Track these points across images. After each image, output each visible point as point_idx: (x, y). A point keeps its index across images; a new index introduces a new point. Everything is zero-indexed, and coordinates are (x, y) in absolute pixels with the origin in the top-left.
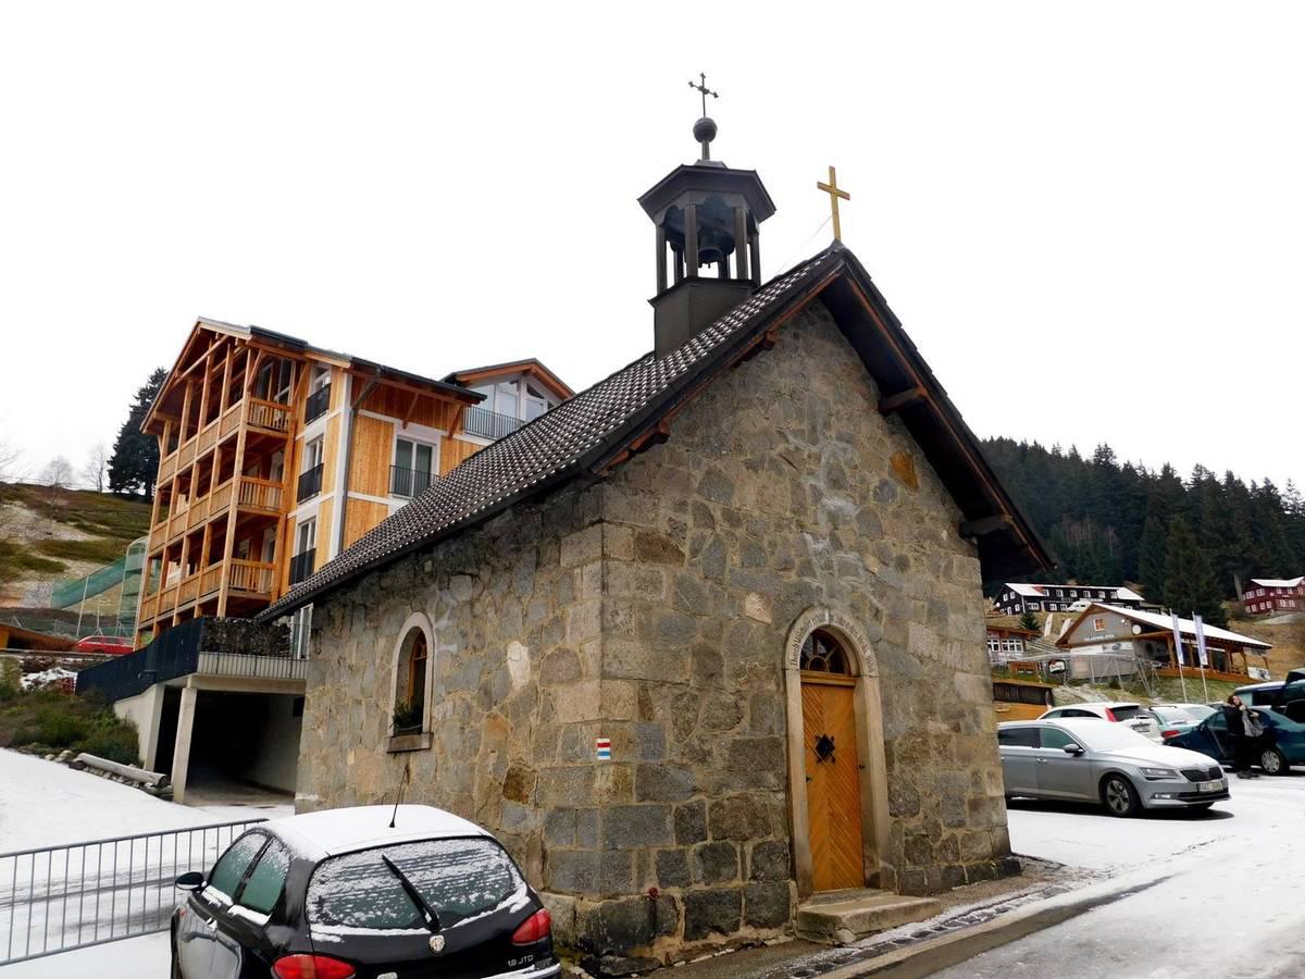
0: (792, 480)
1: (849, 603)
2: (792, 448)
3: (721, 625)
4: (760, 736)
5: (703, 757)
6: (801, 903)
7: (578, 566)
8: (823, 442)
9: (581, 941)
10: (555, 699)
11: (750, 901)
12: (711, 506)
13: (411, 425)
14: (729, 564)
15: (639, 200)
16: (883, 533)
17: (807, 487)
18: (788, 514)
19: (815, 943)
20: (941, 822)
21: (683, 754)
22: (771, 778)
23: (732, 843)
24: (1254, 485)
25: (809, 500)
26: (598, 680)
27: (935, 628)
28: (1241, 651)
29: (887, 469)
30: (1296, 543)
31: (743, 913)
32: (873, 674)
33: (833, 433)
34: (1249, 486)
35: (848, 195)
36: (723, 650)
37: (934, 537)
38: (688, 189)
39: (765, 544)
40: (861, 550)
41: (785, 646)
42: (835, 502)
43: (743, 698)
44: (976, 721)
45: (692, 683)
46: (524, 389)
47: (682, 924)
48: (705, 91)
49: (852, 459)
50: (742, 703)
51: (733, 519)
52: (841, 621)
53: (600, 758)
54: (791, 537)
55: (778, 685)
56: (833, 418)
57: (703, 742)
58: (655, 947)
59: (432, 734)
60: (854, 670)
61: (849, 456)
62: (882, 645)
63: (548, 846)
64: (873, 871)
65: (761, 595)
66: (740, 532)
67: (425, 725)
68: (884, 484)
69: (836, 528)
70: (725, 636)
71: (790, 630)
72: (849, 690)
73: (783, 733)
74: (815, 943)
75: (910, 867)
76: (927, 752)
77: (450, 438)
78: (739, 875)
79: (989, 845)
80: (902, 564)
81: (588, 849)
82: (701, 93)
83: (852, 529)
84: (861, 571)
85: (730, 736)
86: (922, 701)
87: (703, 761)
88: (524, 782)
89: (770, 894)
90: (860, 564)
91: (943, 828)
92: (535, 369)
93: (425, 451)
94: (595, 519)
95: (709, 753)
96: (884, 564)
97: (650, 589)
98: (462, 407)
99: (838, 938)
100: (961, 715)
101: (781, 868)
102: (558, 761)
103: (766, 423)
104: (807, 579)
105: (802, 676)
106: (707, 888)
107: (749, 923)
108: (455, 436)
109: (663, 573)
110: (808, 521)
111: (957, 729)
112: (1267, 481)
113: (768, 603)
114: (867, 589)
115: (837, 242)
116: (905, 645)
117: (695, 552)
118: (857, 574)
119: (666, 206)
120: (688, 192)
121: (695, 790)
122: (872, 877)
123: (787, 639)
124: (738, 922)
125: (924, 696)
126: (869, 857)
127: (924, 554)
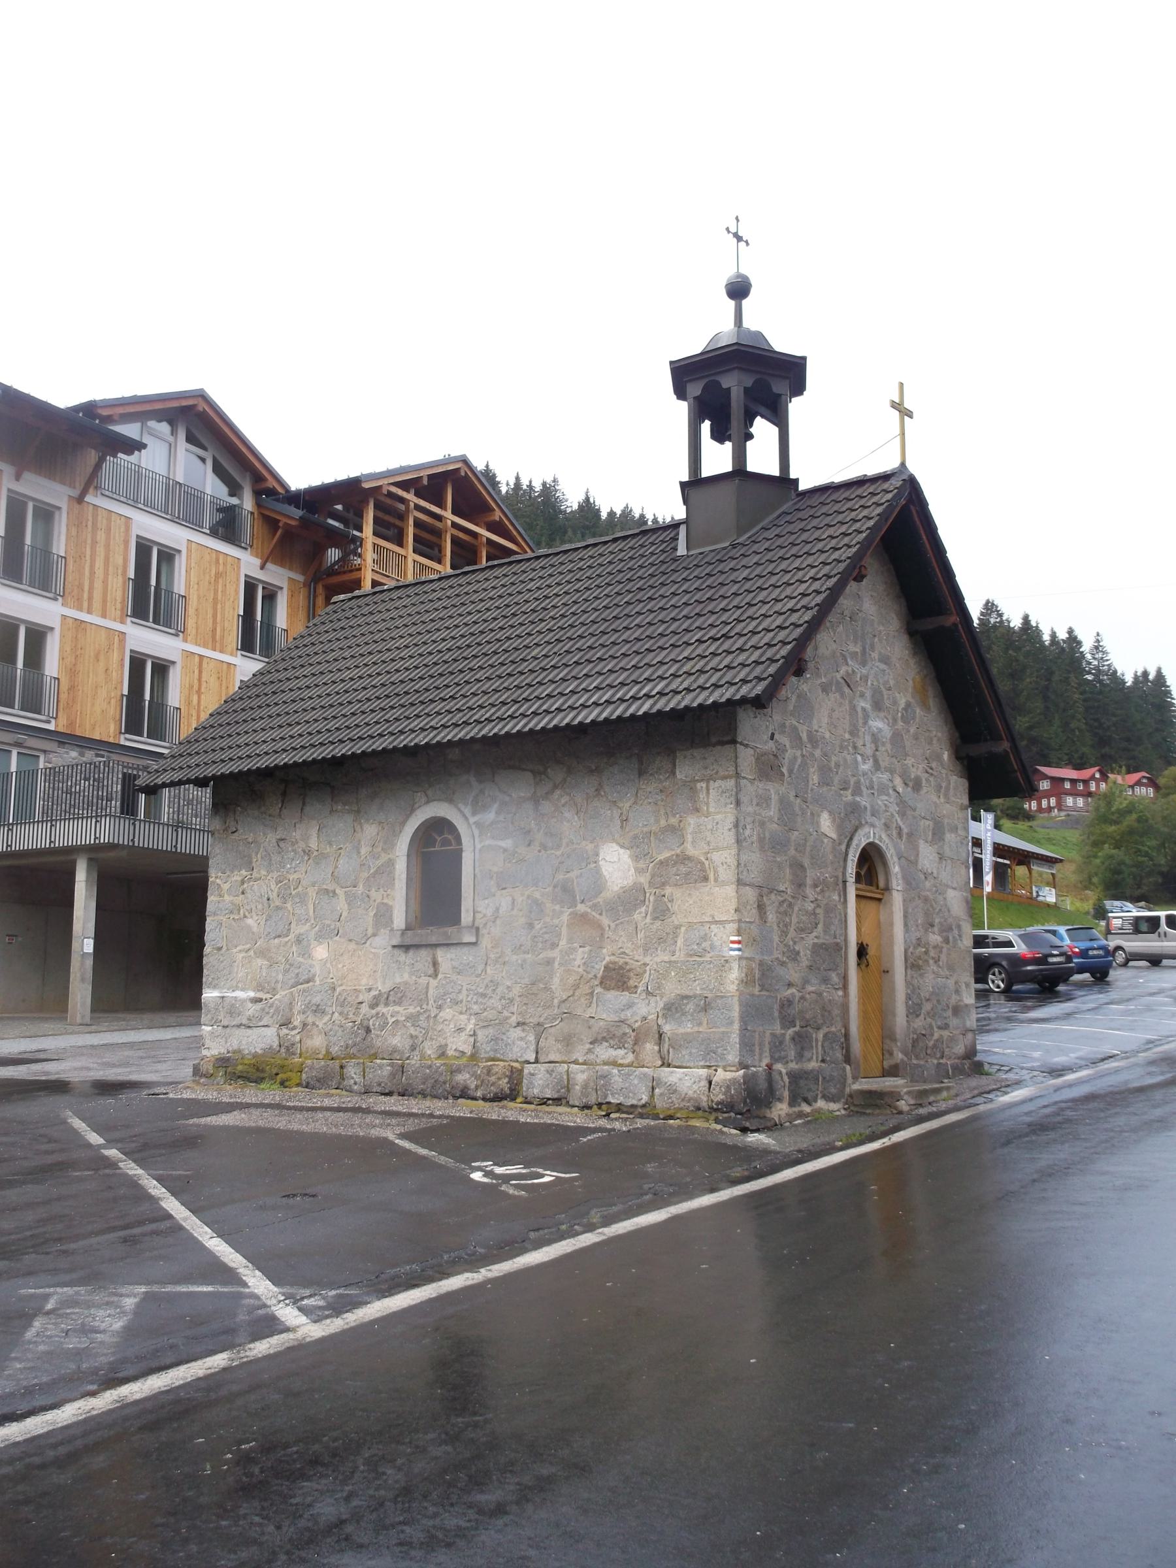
0: (850, 702)
1: (883, 821)
2: (850, 669)
3: (805, 840)
4: (829, 940)
5: (794, 956)
6: (854, 1083)
7: (702, 780)
8: (870, 664)
9: (718, 1103)
10: (671, 901)
11: (824, 1078)
12: (800, 727)
13: (27, 476)
14: (811, 782)
15: (671, 363)
16: (907, 755)
17: (859, 710)
18: (847, 736)
19: (864, 1113)
20: (934, 1024)
21: (784, 953)
22: (834, 977)
23: (811, 1030)
24: (1053, 635)
25: (861, 721)
26: (734, 886)
27: (936, 846)
28: (1028, 865)
29: (910, 690)
30: (1095, 720)
31: (820, 1089)
32: (899, 888)
33: (875, 655)
34: (1046, 638)
35: (893, 407)
36: (806, 862)
37: (938, 758)
38: (740, 369)
39: (833, 764)
40: (892, 771)
41: (845, 860)
42: (877, 724)
43: (818, 906)
44: (960, 936)
45: (789, 891)
46: (182, 435)
47: (786, 1094)
48: (739, 238)
49: (888, 681)
50: (818, 911)
51: (814, 740)
52: (880, 839)
53: (732, 953)
54: (848, 757)
55: (840, 896)
56: (876, 639)
57: (795, 943)
58: (773, 1109)
59: (478, 929)
60: (882, 884)
61: (886, 678)
62: (903, 860)
63: (667, 1028)
64: (892, 1062)
65: (830, 813)
66: (818, 753)
67: (466, 918)
68: (908, 705)
69: (877, 750)
70: (808, 849)
71: (848, 846)
72: (877, 902)
73: (843, 938)
74: (864, 1113)
75: (915, 1062)
76: (927, 961)
77: (80, 500)
78: (814, 1058)
79: (963, 1048)
80: (917, 786)
81: (722, 1029)
82: (735, 240)
83: (887, 751)
84: (891, 791)
85: (811, 940)
86: (927, 914)
87: (795, 959)
88: (632, 974)
89: (835, 1074)
90: (891, 785)
91: (936, 1029)
92: (203, 405)
93: (46, 515)
94: (726, 739)
95: (798, 953)
96: (906, 784)
97: (764, 805)
98: (102, 460)
99: (896, 1108)
100: (950, 929)
101: (839, 1055)
102: (680, 956)
103: (834, 646)
104: (858, 799)
105: (857, 889)
106: (796, 1067)
107: (825, 1097)
108: (89, 498)
109: (772, 791)
110: (859, 743)
111: (947, 941)
112: (1070, 631)
113: (834, 820)
114: (894, 808)
115: (903, 464)
116: (916, 863)
117: (791, 771)
118: (888, 795)
119: (707, 376)
120: (736, 372)
121: (790, 985)
122: (891, 1067)
123: (847, 854)
124: (817, 1095)
125: (928, 910)
126: (888, 1051)
127: (932, 775)
